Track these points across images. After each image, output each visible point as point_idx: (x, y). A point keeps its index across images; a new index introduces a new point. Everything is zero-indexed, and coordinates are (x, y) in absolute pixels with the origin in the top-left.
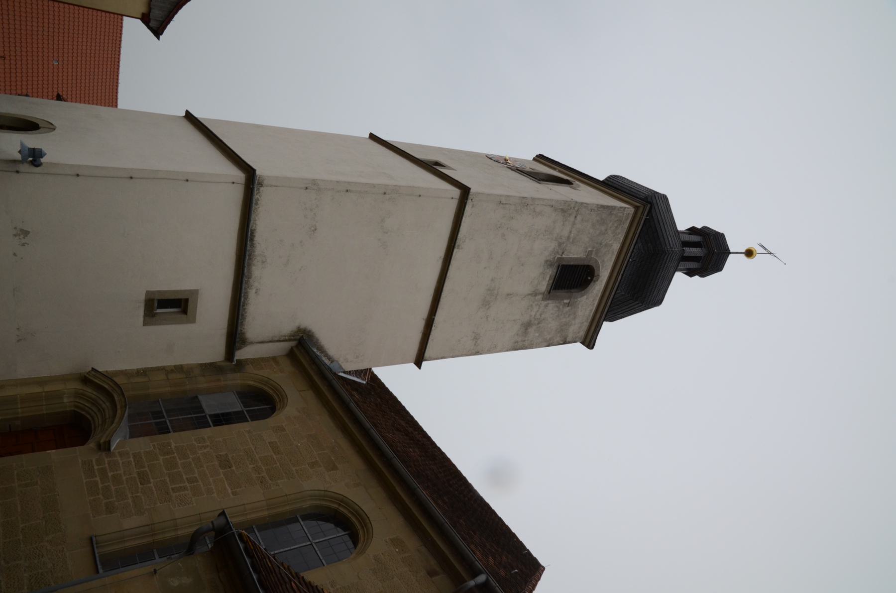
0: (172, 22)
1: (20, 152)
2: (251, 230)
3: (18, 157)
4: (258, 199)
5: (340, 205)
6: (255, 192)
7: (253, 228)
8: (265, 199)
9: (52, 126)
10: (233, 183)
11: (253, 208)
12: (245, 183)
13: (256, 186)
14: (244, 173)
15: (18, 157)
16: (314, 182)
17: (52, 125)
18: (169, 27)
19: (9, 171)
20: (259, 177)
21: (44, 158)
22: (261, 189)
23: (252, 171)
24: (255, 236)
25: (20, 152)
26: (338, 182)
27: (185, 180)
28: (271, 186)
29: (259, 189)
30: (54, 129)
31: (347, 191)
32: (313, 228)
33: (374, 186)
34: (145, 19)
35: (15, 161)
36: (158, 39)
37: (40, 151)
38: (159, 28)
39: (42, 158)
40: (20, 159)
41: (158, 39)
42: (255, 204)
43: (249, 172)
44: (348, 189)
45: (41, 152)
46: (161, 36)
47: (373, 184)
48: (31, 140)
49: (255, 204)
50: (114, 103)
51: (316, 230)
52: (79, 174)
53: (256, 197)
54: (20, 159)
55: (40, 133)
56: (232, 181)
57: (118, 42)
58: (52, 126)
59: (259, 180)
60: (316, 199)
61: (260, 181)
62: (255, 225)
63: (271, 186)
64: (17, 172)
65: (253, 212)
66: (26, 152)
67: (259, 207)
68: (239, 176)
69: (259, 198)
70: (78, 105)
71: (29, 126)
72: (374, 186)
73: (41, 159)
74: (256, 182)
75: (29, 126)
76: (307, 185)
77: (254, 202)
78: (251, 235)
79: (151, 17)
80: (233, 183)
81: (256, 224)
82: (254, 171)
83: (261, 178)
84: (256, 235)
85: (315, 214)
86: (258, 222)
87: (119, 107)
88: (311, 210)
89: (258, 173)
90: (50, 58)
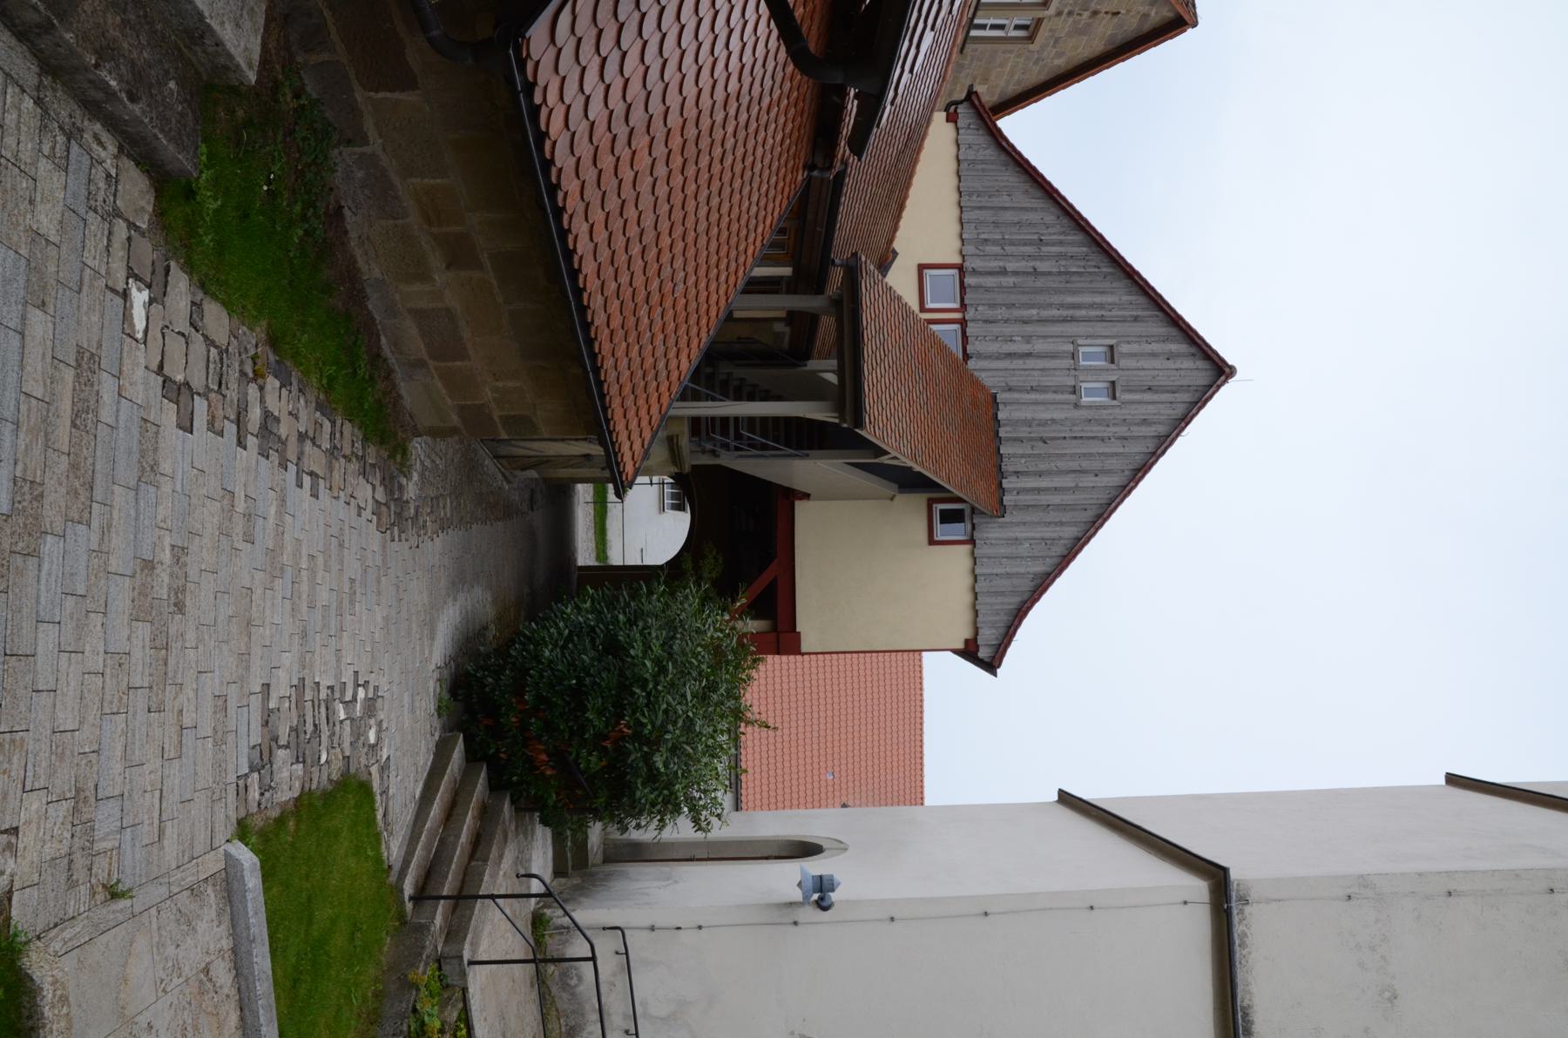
0: (1013, 643)
1: (799, 885)
2: (1243, 1008)
3: (797, 895)
4: (1245, 935)
5: (1440, 930)
6: (1236, 919)
7: (1245, 1004)
8: (1254, 927)
9: (842, 846)
10: (1185, 903)
11: (1238, 955)
12: (1211, 899)
13: (1233, 904)
14: (1205, 880)
15: (797, 895)
16: (1363, 881)
17: (841, 842)
18: (1009, 651)
19: (782, 924)
20: (1238, 885)
21: (837, 891)
22: (1248, 909)
23: (1222, 872)
24: (1252, 1023)
25: (799, 885)
26: (1420, 875)
27: (980, 915)
28: (1269, 901)
29: (1241, 912)
30: (846, 849)
31: (1450, 894)
32: (1387, 994)
33: (1516, 875)
34: (969, 652)
35: (791, 904)
36: (995, 675)
37: (831, 879)
38: (994, 657)
39: (833, 890)
40: (801, 899)
41: (995, 675)
42: (1240, 946)
43: (1217, 876)
44: (1451, 888)
45: (832, 880)
46: (998, 670)
47: (1513, 870)
48: (814, 867)
49: (1240, 946)
50: (919, 801)
51: (1395, 998)
52: (989, 911)
53: (1238, 929)
54: (801, 899)
55: (825, 858)
56: (982, 912)
57: (918, 715)
58: (842, 846)
59: (1238, 891)
60: (1377, 921)
61: (1241, 893)
62: (1248, 996)
63: (1269, 901)
64: (795, 923)
65: (1237, 963)
66: (809, 884)
67: (1250, 953)
68: (1198, 888)
69: (1246, 930)
70: (877, 809)
71: (807, 850)
72: (1517, 876)
73: (831, 894)
74: (1234, 894)
75: (807, 850)
76: (1349, 891)
77: (1237, 942)
78: (1243, 1020)
79: (979, 642)
80: (1185, 903)
81: (1250, 993)
82: (1225, 870)
83: (1241, 886)
84: (1255, 1020)
85: (1383, 958)
86: (1254, 989)
87: (927, 802)
88: (1373, 949)
89: (1234, 875)
90: (823, 771)
